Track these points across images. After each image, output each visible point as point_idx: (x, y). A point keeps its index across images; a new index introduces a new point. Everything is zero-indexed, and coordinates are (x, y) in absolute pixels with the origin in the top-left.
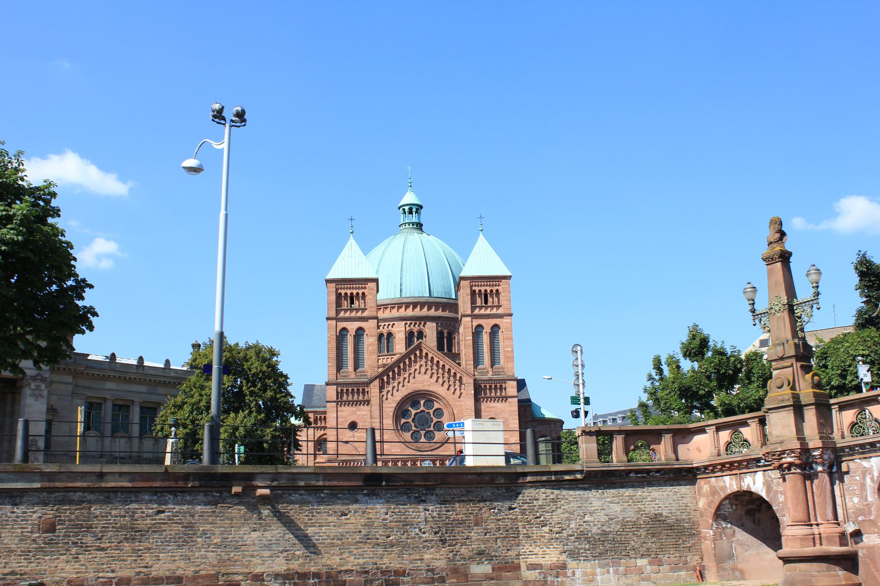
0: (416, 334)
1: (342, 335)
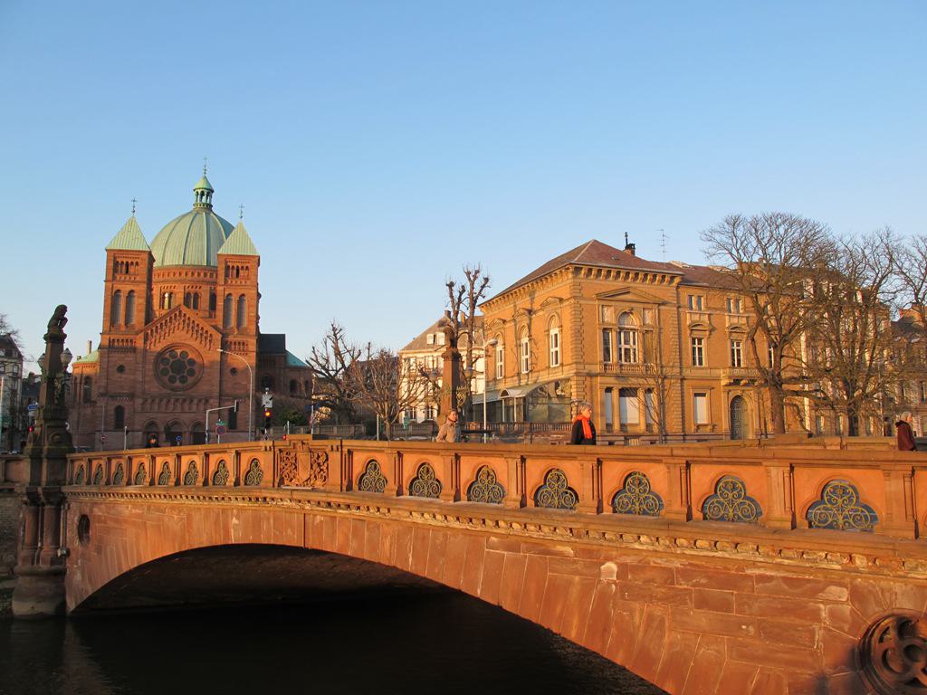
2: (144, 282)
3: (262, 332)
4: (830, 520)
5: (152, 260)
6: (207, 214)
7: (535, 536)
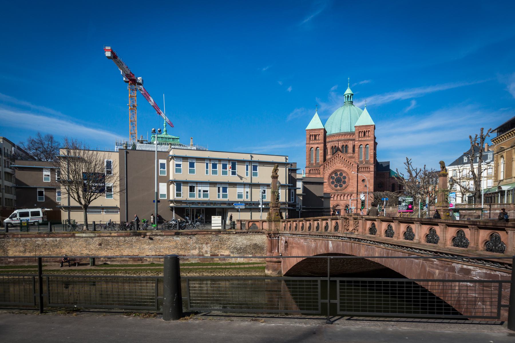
3: (379, 160)
5: (325, 132)
7: (58, 311)
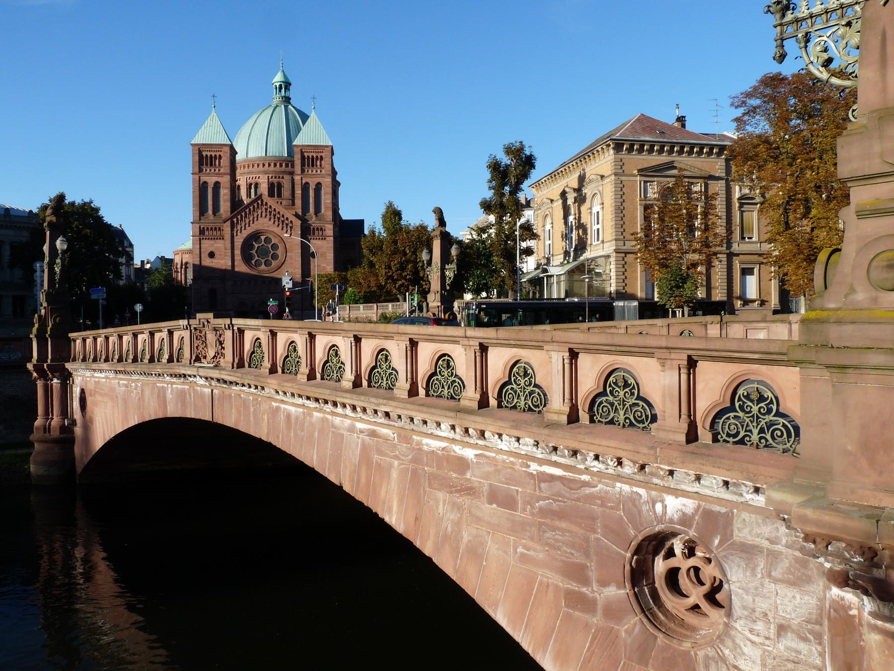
0: (276, 184)
1: (202, 188)
2: (228, 174)
4: (742, 434)
5: (233, 152)
6: (286, 108)
